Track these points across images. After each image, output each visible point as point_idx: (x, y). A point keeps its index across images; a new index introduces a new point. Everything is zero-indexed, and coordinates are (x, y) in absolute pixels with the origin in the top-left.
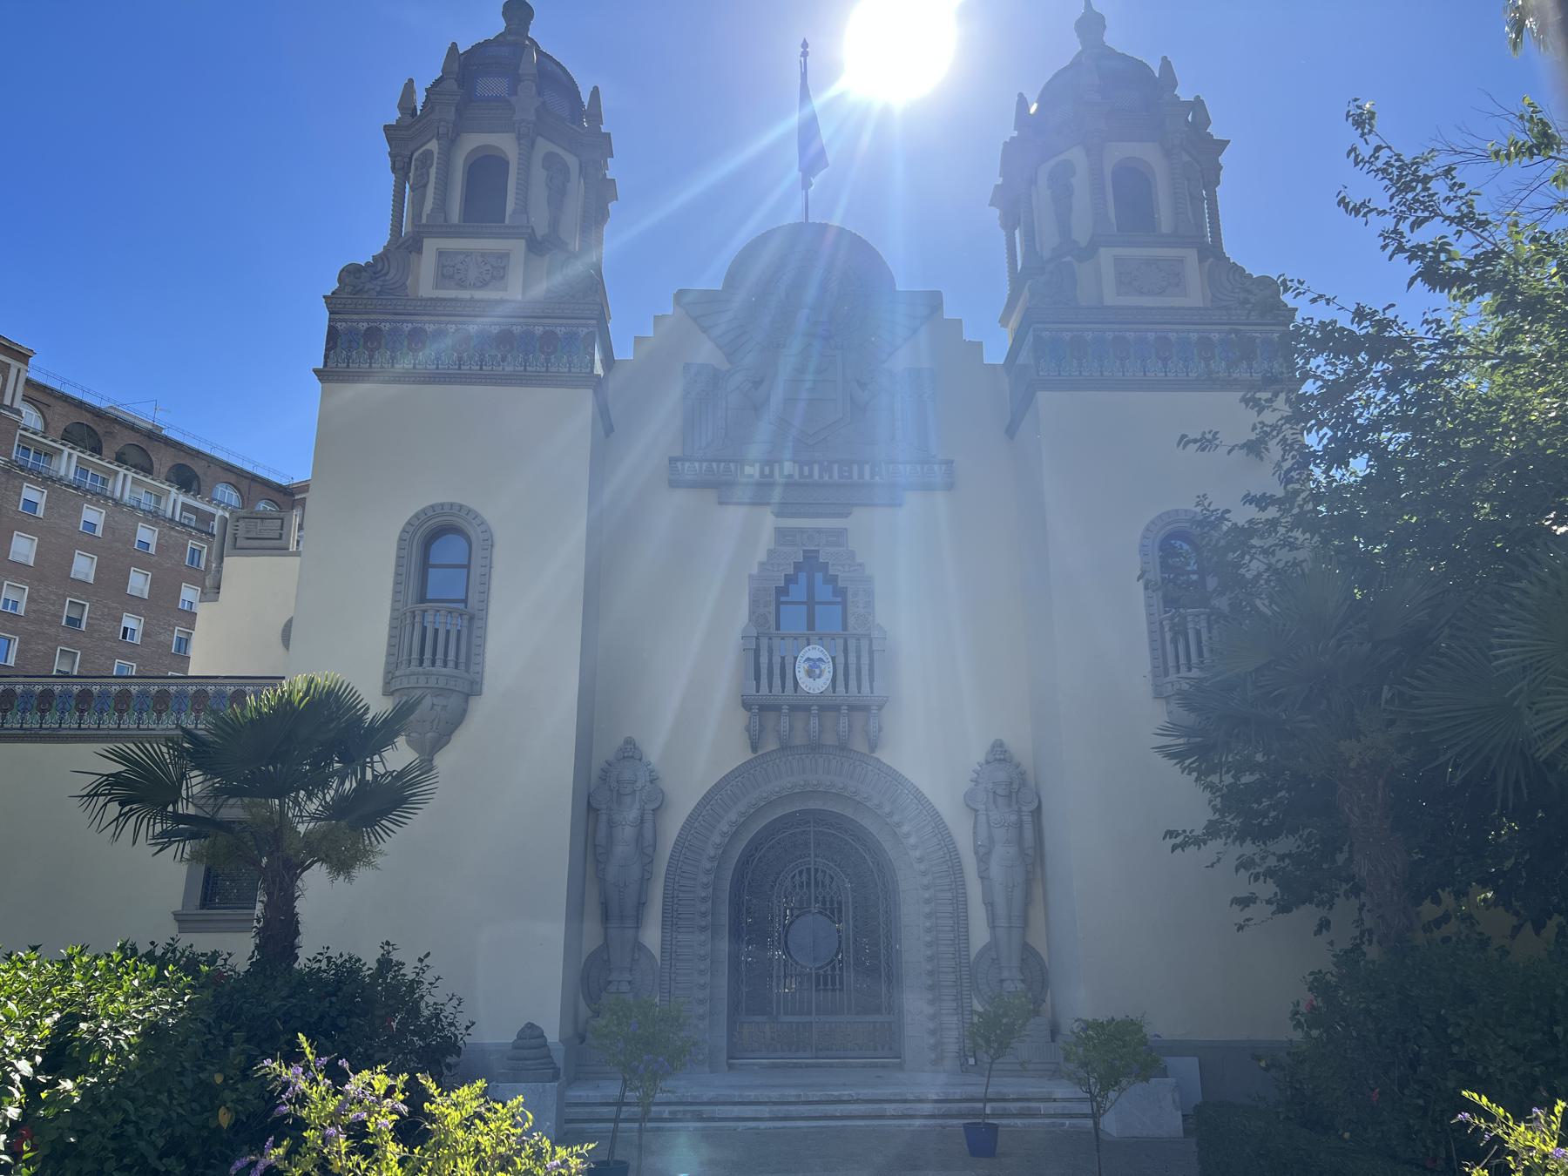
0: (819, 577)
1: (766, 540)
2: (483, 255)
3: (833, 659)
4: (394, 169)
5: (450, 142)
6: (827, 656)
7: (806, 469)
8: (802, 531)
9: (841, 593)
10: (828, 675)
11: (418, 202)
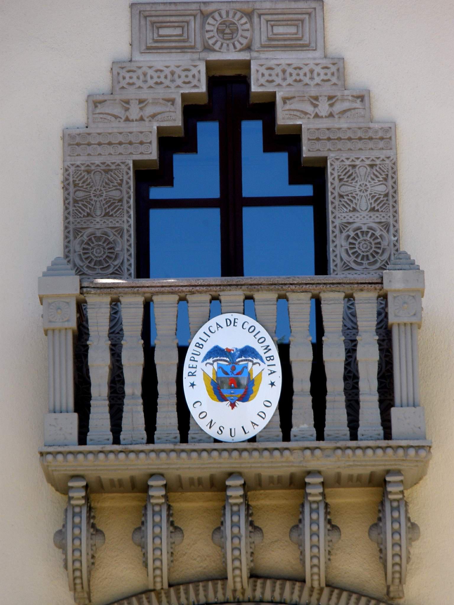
0: (252, 131)
3: (284, 350)
6: (266, 345)
9: (311, 174)
10: (268, 392)
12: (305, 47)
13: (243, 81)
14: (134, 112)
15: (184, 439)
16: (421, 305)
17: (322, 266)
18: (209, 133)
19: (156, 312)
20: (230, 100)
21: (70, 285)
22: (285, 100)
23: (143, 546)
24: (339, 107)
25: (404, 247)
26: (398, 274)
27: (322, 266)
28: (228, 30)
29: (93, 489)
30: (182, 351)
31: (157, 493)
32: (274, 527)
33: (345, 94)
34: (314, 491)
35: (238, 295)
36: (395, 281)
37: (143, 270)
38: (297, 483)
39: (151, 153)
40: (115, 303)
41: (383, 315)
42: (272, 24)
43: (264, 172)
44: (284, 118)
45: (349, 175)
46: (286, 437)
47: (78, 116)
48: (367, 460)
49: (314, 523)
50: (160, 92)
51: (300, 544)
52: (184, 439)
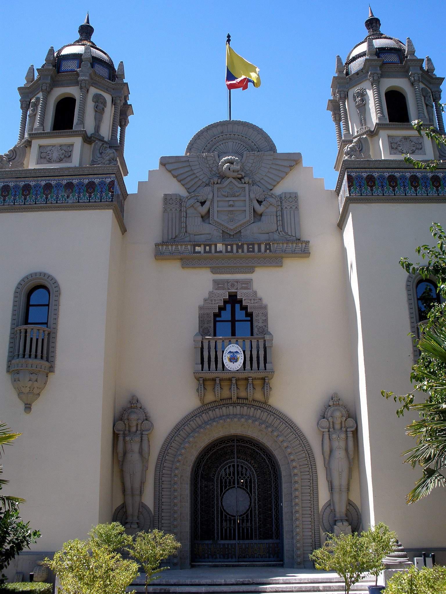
0: (237, 306)
1: (209, 287)
2: (61, 146)
3: (244, 352)
4: (22, 107)
5: (48, 93)
6: (240, 350)
7: (207, 248)
8: (228, 281)
9: (250, 315)
10: (241, 361)
11: (32, 122)
12: (249, 289)
13: (236, 296)
14: (213, 302)
15: (223, 370)
16: (126, 98)
17: (252, 334)
18: (229, 307)
19: (218, 344)
20: (233, 300)
21: (200, 338)
22: (245, 300)
23: (215, 392)
24: (255, 301)
25: (269, 330)
26: (268, 336)
27: (252, 334)
28: (233, 285)
29: (205, 380)
30: (223, 352)
31: (218, 381)
32: (242, 388)
33: (427, 559)
34: (250, 381)
35: (235, 340)
36: (267, 337)
37: (215, 335)
38: (247, 379)
39: (217, 311)
40: (209, 342)
41: (265, 345)
42: (242, 284)
43: (240, 315)
44: (244, 304)
45: (258, 315)
46: (245, 370)
47: (202, 303)
48: (262, 375)
49: (250, 388)
50: (219, 298)
51: (247, 392)
52: (223, 370)
